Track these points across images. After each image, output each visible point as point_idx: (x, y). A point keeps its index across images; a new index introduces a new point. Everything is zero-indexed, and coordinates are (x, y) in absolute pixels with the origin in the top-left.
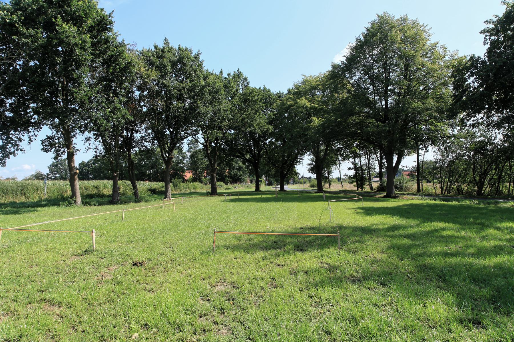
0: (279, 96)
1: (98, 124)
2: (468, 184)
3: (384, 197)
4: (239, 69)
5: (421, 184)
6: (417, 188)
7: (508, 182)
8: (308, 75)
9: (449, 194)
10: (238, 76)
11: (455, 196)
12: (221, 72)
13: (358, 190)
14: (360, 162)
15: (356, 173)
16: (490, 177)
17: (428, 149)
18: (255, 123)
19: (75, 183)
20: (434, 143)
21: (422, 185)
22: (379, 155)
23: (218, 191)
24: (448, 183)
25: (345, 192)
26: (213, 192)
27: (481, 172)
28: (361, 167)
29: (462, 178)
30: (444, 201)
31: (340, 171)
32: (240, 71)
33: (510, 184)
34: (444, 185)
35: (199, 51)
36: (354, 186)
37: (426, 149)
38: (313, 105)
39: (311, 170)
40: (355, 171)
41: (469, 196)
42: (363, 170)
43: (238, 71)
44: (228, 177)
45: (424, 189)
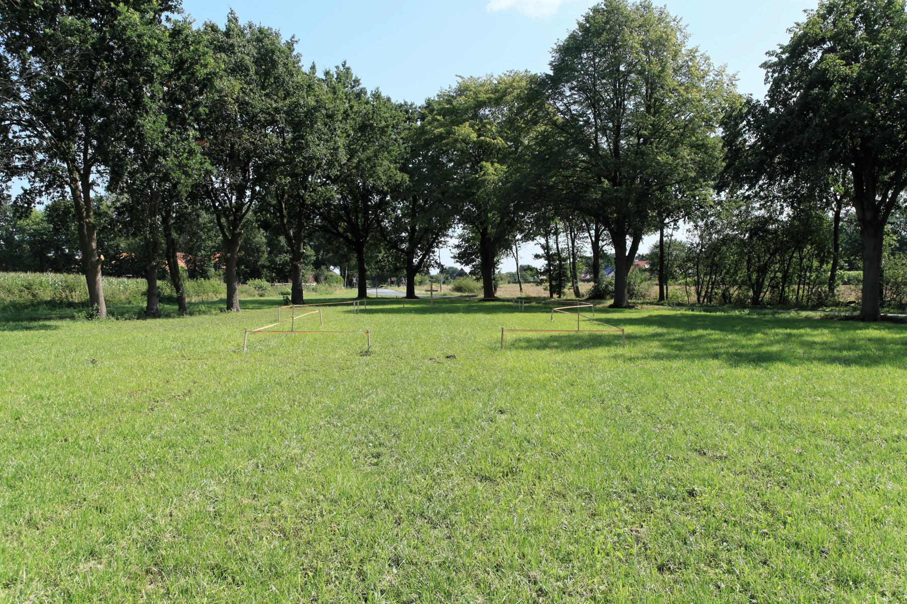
0: (405, 109)
1: (173, 178)
2: (740, 288)
3: (611, 306)
4: (345, 62)
5: (665, 287)
6: (658, 291)
7: (796, 283)
8: (466, 76)
9: (710, 302)
10: (345, 75)
11: (728, 288)
12: (313, 68)
13: (551, 296)
14: (557, 245)
15: (549, 265)
16: (772, 276)
17: (678, 224)
18: (380, 170)
19: (97, 279)
20: (688, 215)
21: (667, 288)
22: (593, 232)
23: (306, 296)
24: (708, 284)
25: (528, 299)
26: (297, 298)
27: (759, 267)
28: (558, 254)
29: (731, 277)
30: (705, 311)
31: (517, 260)
32: (347, 66)
33: (799, 287)
34: (702, 288)
35: (293, 37)
36: (545, 289)
37: (675, 224)
38: (482, 138)
39: (459, 257)
40: (546, 262)
41: (740, 304)
42: (561, 259)
43: (343, 66)
44: (268, 268)
45: (670, 295)
